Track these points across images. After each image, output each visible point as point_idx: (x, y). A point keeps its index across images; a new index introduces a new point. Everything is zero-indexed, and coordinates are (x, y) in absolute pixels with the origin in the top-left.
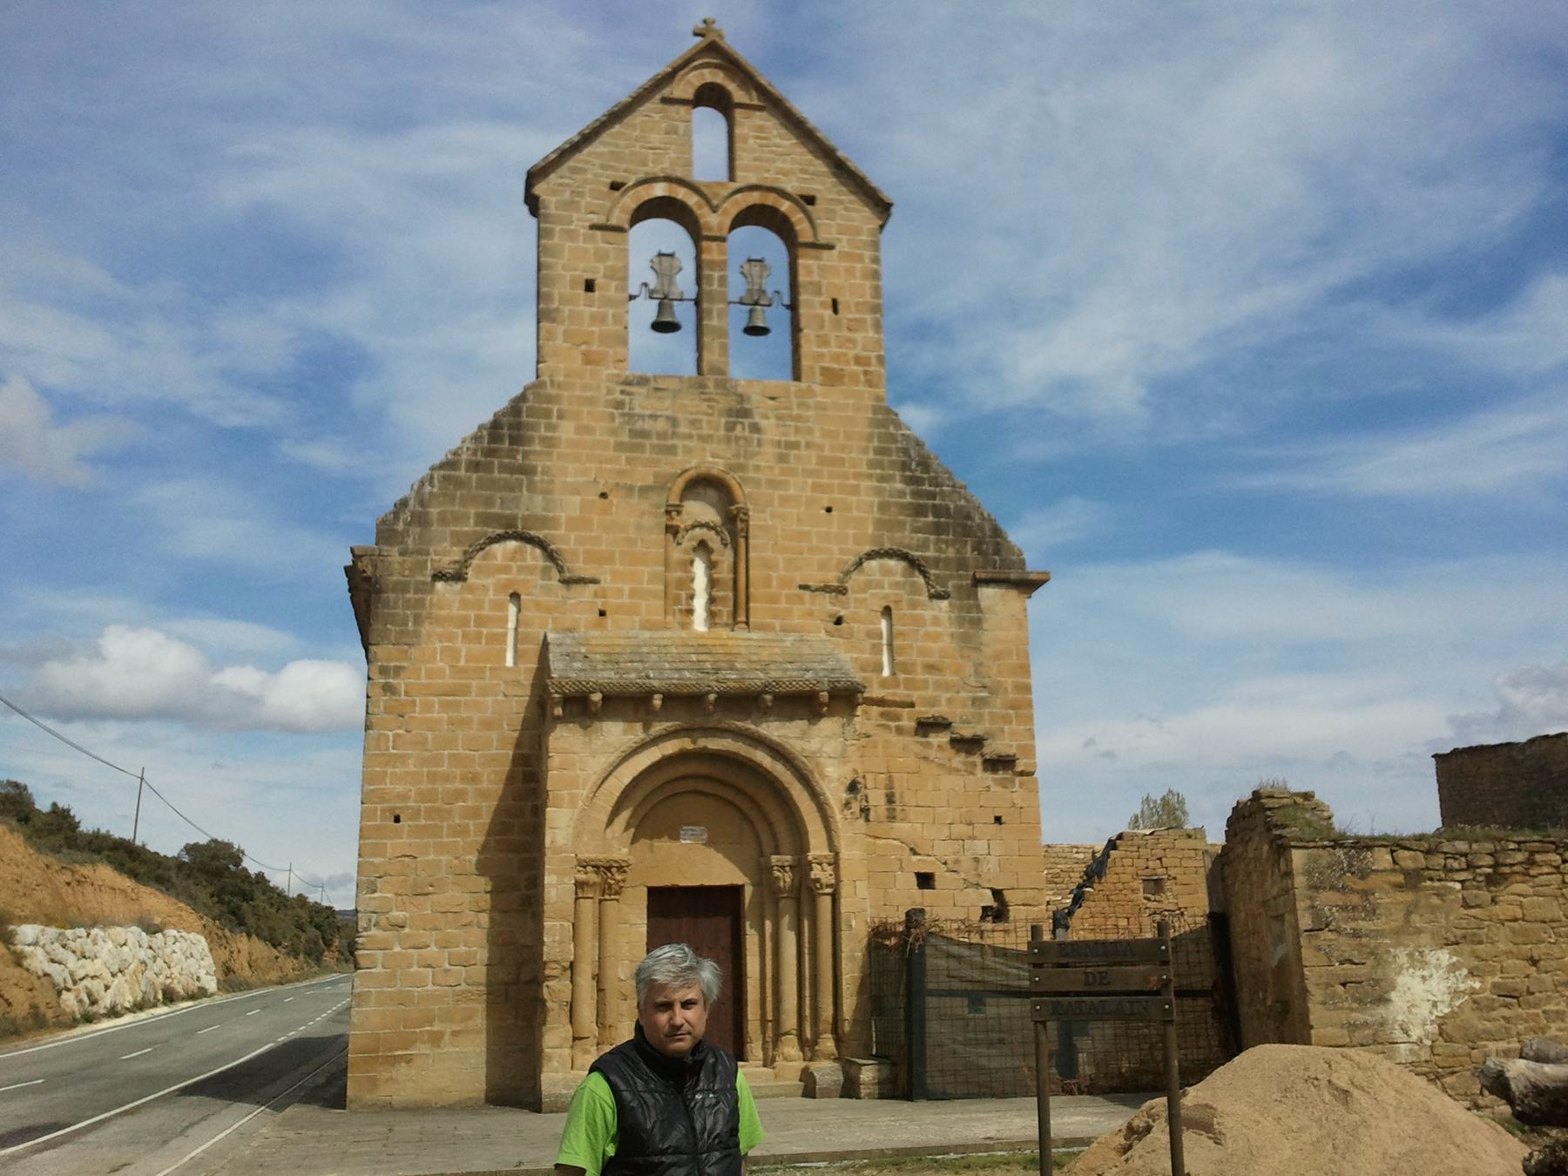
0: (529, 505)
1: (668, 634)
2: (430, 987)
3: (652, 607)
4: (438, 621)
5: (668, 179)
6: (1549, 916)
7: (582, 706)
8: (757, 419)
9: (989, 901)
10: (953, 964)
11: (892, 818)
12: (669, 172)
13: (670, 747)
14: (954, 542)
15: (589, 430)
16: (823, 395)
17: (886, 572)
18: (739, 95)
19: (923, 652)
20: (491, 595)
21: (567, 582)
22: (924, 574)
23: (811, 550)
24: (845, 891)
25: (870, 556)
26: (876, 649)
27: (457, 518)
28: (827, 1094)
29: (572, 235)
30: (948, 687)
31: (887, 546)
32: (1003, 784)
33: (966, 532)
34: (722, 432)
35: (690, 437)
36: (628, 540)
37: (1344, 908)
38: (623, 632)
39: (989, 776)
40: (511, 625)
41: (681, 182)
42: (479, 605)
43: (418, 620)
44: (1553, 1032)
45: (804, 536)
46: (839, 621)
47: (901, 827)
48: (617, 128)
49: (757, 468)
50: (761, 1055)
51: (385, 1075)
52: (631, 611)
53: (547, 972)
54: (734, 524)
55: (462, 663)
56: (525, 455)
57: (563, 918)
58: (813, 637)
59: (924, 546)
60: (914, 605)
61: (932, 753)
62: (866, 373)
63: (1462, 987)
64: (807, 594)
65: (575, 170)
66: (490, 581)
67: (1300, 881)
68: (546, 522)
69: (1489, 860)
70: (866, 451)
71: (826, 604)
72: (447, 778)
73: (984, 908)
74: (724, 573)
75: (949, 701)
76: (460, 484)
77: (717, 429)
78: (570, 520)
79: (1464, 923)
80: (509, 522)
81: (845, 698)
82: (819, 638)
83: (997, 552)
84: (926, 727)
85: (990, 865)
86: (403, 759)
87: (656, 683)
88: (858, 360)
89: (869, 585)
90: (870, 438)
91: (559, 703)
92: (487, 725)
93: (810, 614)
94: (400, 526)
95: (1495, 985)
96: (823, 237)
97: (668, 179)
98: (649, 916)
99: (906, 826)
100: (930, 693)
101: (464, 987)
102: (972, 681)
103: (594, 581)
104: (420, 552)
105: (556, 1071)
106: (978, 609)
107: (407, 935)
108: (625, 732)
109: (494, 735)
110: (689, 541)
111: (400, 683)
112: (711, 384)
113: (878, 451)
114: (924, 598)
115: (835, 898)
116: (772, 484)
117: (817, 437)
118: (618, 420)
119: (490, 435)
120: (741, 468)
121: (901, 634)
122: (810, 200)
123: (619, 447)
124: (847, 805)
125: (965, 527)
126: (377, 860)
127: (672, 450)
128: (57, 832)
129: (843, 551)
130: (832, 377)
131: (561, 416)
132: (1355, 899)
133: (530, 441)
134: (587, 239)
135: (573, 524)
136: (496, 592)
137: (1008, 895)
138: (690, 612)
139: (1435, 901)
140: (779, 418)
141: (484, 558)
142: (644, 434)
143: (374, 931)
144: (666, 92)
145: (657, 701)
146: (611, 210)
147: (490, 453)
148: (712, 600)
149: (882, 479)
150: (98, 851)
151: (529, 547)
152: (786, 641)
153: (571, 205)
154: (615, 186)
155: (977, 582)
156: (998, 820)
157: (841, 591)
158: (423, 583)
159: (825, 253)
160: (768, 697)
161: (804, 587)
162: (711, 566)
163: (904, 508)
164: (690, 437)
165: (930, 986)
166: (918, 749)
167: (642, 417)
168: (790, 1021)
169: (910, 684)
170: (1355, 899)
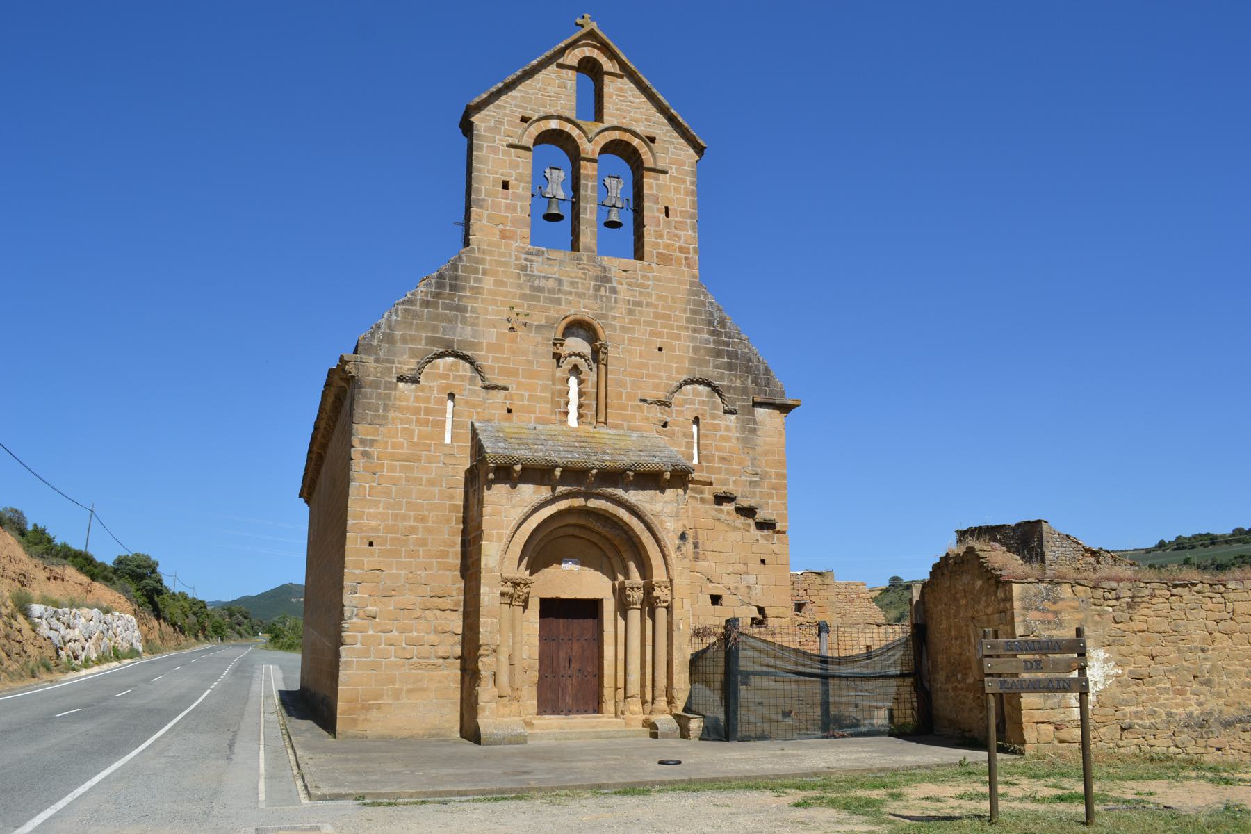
0: (461, 333)
1: (553, 427)
2: (392, 659)
3: (543, 408)
4: (400, 409)
5: (560, 118)
6: (1162, 630)
7: (507, 474)
8: (615, 284)
9: (756, 614)
10: (757, 654)
11: (696, 558)
12: (561, 113)
13: (563, 505)
14: (741, 376)
15: (503, 284)
16: (657, 271)
17: (697, 394)
18: (608, 65)
19: (718, 449)
20: (435, 394)
21: (486, 388)
22: (720, 395)
23: (648, 376)
24: (676, 605)
25: (687, 382)
26: (689, 445)
27: (414, 339)
28: (666, 736)
29: (495, 150)
30: (734, 473)
31: (698, 376)
32: (766, 538)
33: (748, 370)
34: (591, 292)
35: (570, 293)
36: (528, 361)
37: (1043, 622)
38: (522, 423)
39: (758, 533)
40: (449, 415)
41: (626, 130)
42: (427, 400)
43: (386, 408)
44: (1161, 701)
45: (645, 366)
46: (665, 425)
47: (702, 565)
48: (529, 82)
49: (614, 318)
50: (613, 709)
51: (362, 717)
52: (529, 410)
53: (481, 652)
54: (598, 355)
55: (415, 440)
56: (461, 298)
57: (493, 617)
58: (648, 434)
59: (721, 378)
60: (714, 417)
61: (723, 517)
62: (686, 258)
63: (1112, 672)
64: (646, 405)
65: (500, 107)
66: (435, 384)
67: (1017, 604)
68: (473, 345)
69: (1130, 594)
70: (685, 311)
71: (657, 413)
72: (404, 518)
73: (753, 619)
74: (590, 387)
75: (734, 482)
76: (416, 315)
77: (588, 289)
78: (489, 344)
79: (1113, 633)
80: (449, 343)
81: (680, 478)
82: (654, 437)
83: (767, 385)
84: (720, 499)
85: (757, 591)
86: (375, 504)
87: (558, 460)
88: (681, 249)
89: (685, 402)
90: (688, 302)
91: (486, 471)
92: (431, 483)
93: (647, 419)
94: (375, 342)
95: (1130, 672)
96: (661, 166)
97: (560, 118)
98: (541, 616)
99: (705, 564)
100: (723, 476)
101: (415, 659)
102: (749, 469)
103: (506, 389)
104: (388, 361)
105: (488, 717)
106: (755, 422)
107: (378, 624)
108: (535, 493)
109: (436, 490)
110: (566, 365)
111: (374, 451)
112: (585, 258)
113: (694, 312)
114: (721, 412)
115: (669, 609)
116: (623, 329)
117: (653, 300)
118: (523, 279)
119: (437, 283)
120: (604, 317)
121: (706, 436)
122: (652, 140)
123: (523, 297)
124: (679, 548)
125: (747, 367)
126: (357, 572)
127: (558, 302)
128: (40, 544)
129: (669, 378)
130: (664, 260)
131: (484, 273)
132: (1050, 616)
133: (464, 288)
134: (505, 154)
135: (491, 348)
136: (439, 392)
137: (767, 611)
138: (567, 413)
139: (1097, 618)
140: (629, 284)
141: (431, 368)
142: (540, 289)
143: (355, 620)
144: (561, 61)
145: (558, 472)
146: (522, 135)
147: (437, 295)
148: (580, 406)
149: (695, 331)
150: (65, 557)
151: (462, 362)
152: (630, 439)
153: (495, 130)
154: (524, 120)
155: (755, 404)
156: (763, 562)
157: (668, 405)
158: (390, 383)
159: (661, 176)
160: (631, 473)
161: (644, 401)
162: (580, 382)
163: (709, 351)
164: (570, 293)
165: (741, 668)
166: (714, 513)
167: (539, 277)
168: (634, 688)
169: (710, 470)
170: (1050, 616)
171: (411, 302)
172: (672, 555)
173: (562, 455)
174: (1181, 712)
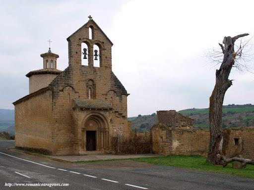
0: (70, 82)
3: (85, 96)
27: (62, 83)
68: (72, 84)
84: (116, 112)
122: (103, 43)
147: (66, 75)
152: (99, 102)
162: (91, 90)
168: (102, 146)
171: (61, 76)
172: (109, 123)
173: (86, 105)
174: (188, 150)
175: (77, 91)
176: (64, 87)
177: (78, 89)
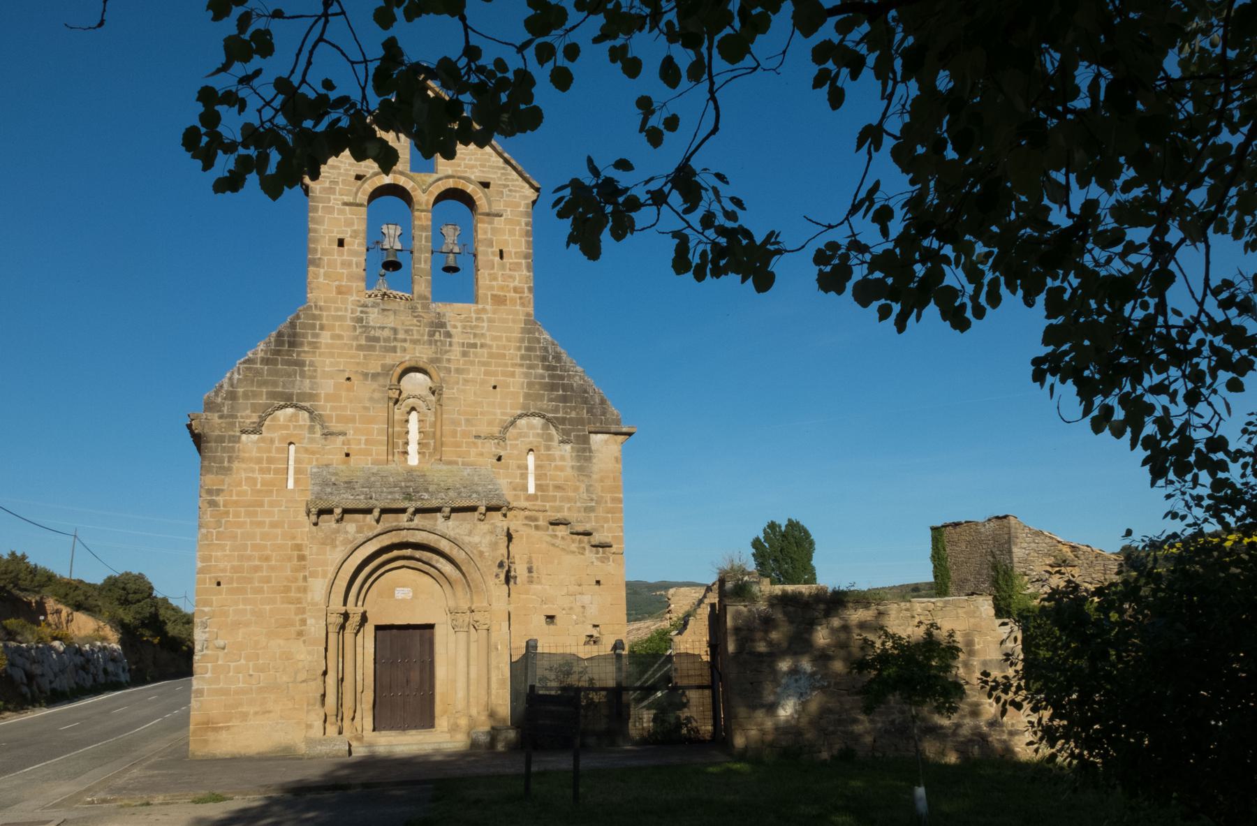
68: (312, 397)
122: (486, 185)
147: (278, 352)
175: (335, 426)
176: (266, 413)
177: (340, 419)
